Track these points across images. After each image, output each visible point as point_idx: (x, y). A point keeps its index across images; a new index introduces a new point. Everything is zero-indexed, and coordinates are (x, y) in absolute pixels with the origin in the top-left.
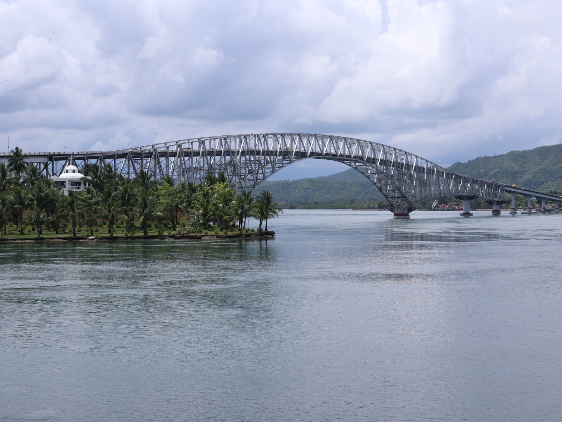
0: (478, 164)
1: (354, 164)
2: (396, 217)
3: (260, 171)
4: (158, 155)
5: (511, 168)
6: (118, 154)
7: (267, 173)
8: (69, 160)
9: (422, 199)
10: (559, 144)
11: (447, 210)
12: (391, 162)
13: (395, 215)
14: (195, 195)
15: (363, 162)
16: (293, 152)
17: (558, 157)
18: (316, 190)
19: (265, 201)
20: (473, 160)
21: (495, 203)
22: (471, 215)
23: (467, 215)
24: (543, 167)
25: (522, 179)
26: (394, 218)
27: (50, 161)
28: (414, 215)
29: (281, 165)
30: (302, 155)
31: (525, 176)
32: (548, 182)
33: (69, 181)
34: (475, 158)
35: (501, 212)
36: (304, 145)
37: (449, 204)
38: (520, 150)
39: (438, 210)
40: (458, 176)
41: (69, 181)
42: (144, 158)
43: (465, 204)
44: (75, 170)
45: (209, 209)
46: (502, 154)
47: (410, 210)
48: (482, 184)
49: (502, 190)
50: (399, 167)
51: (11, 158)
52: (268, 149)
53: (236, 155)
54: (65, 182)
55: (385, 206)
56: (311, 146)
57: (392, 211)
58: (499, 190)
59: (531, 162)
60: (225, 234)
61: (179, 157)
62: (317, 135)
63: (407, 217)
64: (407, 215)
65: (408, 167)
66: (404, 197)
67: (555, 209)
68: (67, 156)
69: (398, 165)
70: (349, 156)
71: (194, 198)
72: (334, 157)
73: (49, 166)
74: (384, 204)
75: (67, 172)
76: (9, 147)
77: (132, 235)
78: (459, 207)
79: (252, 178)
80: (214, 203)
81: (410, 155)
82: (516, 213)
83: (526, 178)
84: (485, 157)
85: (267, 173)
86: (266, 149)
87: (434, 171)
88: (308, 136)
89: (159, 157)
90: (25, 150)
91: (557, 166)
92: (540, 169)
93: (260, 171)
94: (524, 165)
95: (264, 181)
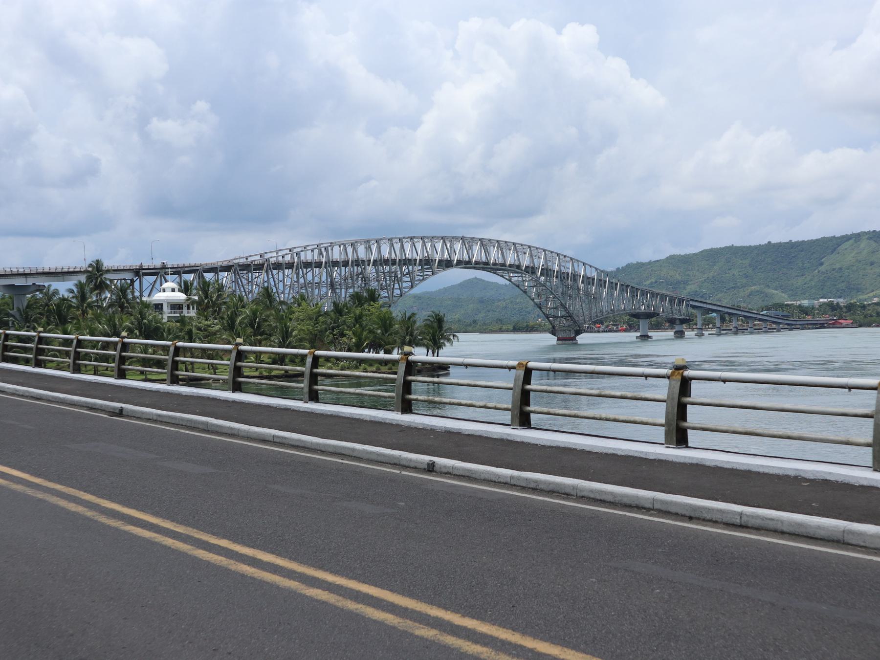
0: (628, 272)
1: (507, 275)
2: (560, 342)
3: (397, 286)
4: (272, 267)
5: (671, 277)
6: (221, 267)
7: (404, 288)
8: (161, 275)
9: (592, 319)
10: (731, 245)
11: (603, 332)
12: (554, 271)
13: (558, 340)
14: (343, 319)
15: (521, 271)
16: (436, 260)
17: (729, 262)
18: (422, 309)
19: (435, 325)
20: (622, 267)
21: (678, 322)
22: (650, 337)
23: (645, 337)
24: (711, 274)
25: (686, 290)
26: (558, 344)
27: (137, 277)
28: (582, 339)
29: (422, 278)
30: (447, 264)
31: (689, 287)
32: (718, 293)
33: (168, 303)
34: (624, 265)
35: (686, 333)
36: (428, 250)
37: (605, 324)
38: (682, 254)
39: (591, 332)
40: (634, 288)
41: (168, 303)
42: (255, 271)
43: (643, 324)
44: (174, 289)
45: (363, 337)
46: (659, 259)
47: (578, 332)
48: (663, 297)
49: (687, 305)
50: (564, 277)
51: (89, 274)
52: (358, 258)
53: (367, 265)
54: (162, 305)
55: (522, 327)
56: (459, 252)
57: (554, 333)
58: (683, 305)
59: (697, 268)
60: (389, 370)
61: (297, 269)
62: (465, 237)
63: (574, 342)
64: (574, 339)
65: (575, 277)
66: (570, 316)
67: (749, 328)
68: (158, 271)
69: (562, 276)
70: (504, 265)
71: (343, 323)
72: (485, 266)
73: (135, 283)
74: (521, 326)
75: (164, 291)
76: (85, 259)
77: (269, 373)
78: (617, 328)
79: (386, 295)
80: (369, 328)
81: (576, 261)
82: (703, 335)
83: (691, 289)
84: (638, 263)
85: (404, 288)
86: (404, 258)
87: (605, 282)
88: (432, 238)
89: (272, 269)
90: (107, 264)
91: (729, 273)
92: (708, 278)
93: (397, 286)
94: (688, 272)
95: (401, 298)
